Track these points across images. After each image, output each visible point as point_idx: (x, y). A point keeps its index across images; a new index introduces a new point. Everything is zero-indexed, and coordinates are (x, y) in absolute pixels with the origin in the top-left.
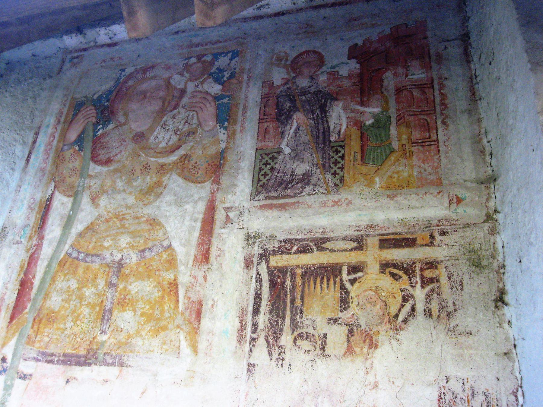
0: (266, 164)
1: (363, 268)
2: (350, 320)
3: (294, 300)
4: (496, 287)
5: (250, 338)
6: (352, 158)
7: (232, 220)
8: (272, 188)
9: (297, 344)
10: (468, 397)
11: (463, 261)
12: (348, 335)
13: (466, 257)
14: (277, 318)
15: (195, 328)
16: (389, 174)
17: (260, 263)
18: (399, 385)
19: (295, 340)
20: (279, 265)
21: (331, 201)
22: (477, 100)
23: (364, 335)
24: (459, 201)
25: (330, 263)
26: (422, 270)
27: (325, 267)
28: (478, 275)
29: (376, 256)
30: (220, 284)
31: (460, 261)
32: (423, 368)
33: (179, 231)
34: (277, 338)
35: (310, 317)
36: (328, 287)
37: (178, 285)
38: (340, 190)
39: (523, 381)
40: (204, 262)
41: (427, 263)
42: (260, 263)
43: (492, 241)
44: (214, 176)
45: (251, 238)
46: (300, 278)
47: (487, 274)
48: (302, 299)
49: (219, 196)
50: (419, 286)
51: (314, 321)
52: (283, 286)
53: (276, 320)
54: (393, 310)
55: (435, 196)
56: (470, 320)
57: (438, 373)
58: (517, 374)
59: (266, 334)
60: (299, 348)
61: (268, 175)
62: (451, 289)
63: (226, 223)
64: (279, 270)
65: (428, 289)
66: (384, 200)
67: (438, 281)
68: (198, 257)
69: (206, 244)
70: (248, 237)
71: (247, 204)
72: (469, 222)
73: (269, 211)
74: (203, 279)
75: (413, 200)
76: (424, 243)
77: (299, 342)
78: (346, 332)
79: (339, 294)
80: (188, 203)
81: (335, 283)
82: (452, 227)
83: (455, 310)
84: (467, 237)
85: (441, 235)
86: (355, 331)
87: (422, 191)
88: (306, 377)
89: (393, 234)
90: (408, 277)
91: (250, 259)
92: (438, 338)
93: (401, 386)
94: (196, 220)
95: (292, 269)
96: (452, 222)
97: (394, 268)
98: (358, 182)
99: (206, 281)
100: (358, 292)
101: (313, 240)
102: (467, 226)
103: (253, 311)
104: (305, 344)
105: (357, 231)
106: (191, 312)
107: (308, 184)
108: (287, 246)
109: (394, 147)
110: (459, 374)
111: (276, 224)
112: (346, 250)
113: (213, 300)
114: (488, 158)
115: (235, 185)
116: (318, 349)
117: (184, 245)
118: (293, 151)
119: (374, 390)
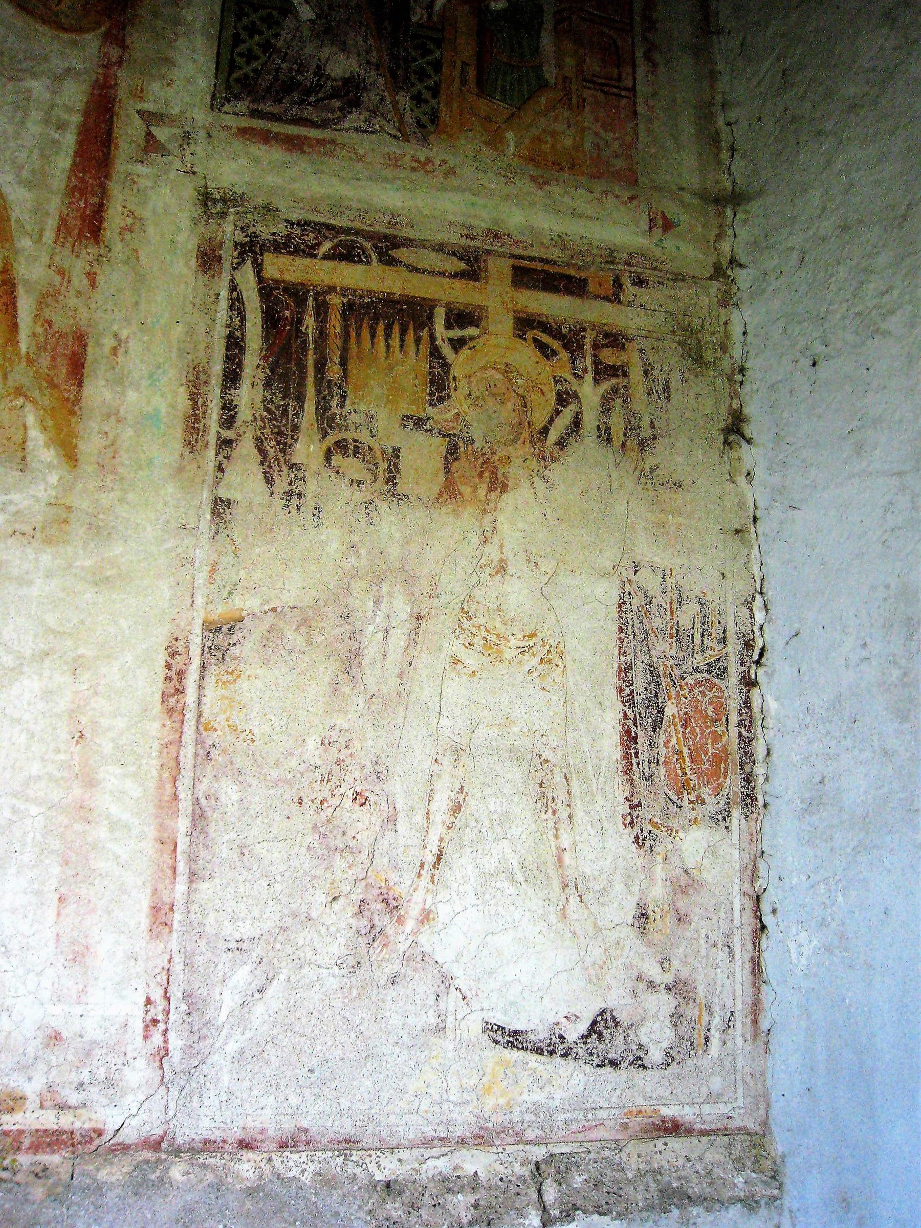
0: (252, 30)
1: (480, 319)
2: (451, 425)
3: (324, 365)
4: (727, 405)
5: (218, 439)
6: (456, 73)
7: (164, 147)
8: (268, 89)
9: (333, 463)
10: (671, 603)
11: (670, 344)
12: (446, 457)
13: (677, 338)
14: (283, 398)
15: (68, 399)
16: (536, 131)
17: (239, 264)
18: (548, 571)
19: (328, 455)
20: (288, 277)
21: (408, 157)
22: (711, 32)
23: (481, 461)
24: (668, 226)
25: (407, 296)
26: (596, 346)
27: (398, 302)
28: (696, 376)
29: (506, 299)
30: (134, 300)
31: (667, 344)
32: (593, 540)
33: (12, 144)
34: (285, 444)
35: (362, 407)
36: (402, 346)
37: (14, 286)
38: (432, 138)
39: (765, 583)
40: (87, 238)
41: (607, 335)
42: (239, 264)
43: (723, 319)
44: (108, 24)
45: (215, 201)
46: (339, 317)
47: (712, 379)
48: (343, 363)
49: (125, 79)
50: (589, 377)
51: (372, 417)
52: (298, 331)
53: (282, 403)
54: (539, 418)
55: (624, 203)
56: (680, 459)
57: (619, 556)
58: (755, 569)
59: (258, 433)
60: (338, 472)
61: (257, 58)
62: (649, 394)
63: (146, 150)
64: (286, 290)
65: (606, 386)
66: (524, 185)
67: (625, 375)
68: (71, 222)
69: (94, 194)
70: (205, 198)
71: (201, 116)
72: (684, 271)
73: (261, 146)
74: (86, 282)
75: (581, 199)
76: (603, 293)
77: (336, 460)
78: (443, 449)
79: (428, 366)
80: (35, 76)
81: (418, 341)
82: (656, 272)
83: (654, 438)
84: (678, 300)
85: (634, 284)
86: (462, 449)
87: (598, 187)
88: (355, 538)
89: (541, 260)
90: (569, 355)
91: (214, 251)
92: (621, 486)
93: (550, 573)
94: (61, 126)
95: (317, 294)
96: (655, 264)
97: (543, 332)
98: (471, 130)
99: (93, 284)
100: (468, 370)
101: (369, 236)
102: (678, 277)
103: (224, 375)
104: (352, 466)
105: (467, 237)
106: (53, 358)
107: (356, 103)
108: (306, 238)
109: (547, 76)
110: (656, 559)
111: (280, 181)
112: (442, 274)
113: (116, 335)
114: (725, 155)
115: (169, 62)
116: (381, 479)
117: (29, 185)
118: (319, 16)
119: (498, 578)
